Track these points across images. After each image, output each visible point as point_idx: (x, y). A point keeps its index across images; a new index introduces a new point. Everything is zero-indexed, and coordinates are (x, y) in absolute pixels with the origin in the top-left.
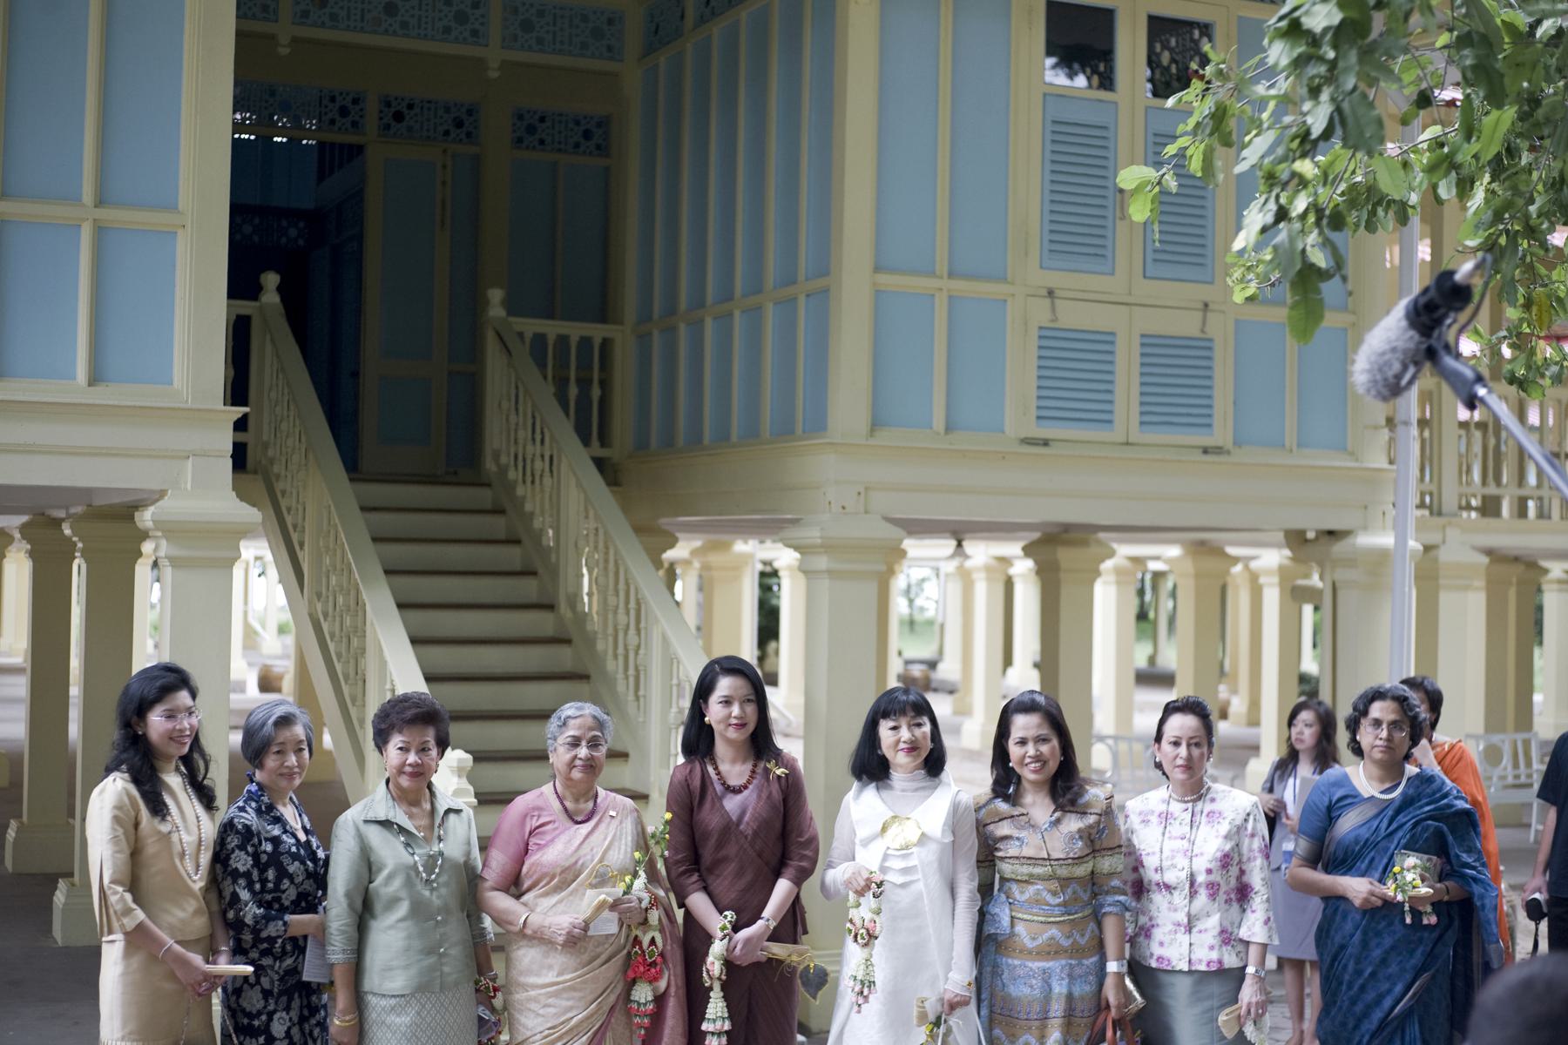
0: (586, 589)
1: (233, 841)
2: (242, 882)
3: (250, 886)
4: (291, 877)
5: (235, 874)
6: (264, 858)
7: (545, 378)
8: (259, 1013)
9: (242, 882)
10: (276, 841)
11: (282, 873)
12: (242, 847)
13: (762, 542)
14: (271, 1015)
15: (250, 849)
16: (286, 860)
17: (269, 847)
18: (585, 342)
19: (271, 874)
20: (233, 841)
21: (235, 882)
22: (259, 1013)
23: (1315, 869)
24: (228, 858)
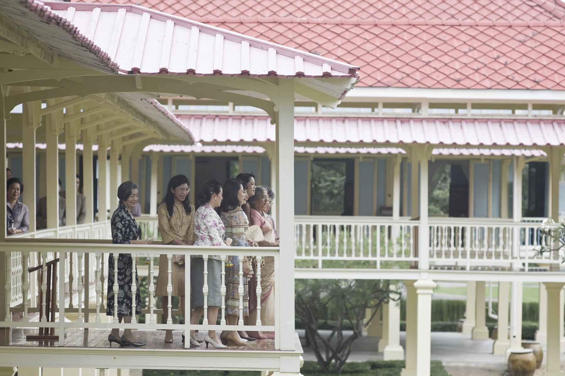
0: (6, 166)
1: (117, 219)
2: (119, 231)
3: (121, 233)
4: (133, 232)
5: (118, 229)
6: (126, 225)
7: (46, 4)
8: (123, 268)
9: (119, 231)
10: (129, 221)
11: (131, 230)
12: (121, 222)
13: (560, 215)
14: (126, 270)
15: (123, 223)
16: (132, 227)
17: (127, 222)
18: (341, 253)
19: (128, 230)
20: (117, 219)
21: (117, 231)
22: (123, 268)
23: (357, 280)
24: (116, 223)
